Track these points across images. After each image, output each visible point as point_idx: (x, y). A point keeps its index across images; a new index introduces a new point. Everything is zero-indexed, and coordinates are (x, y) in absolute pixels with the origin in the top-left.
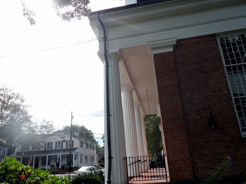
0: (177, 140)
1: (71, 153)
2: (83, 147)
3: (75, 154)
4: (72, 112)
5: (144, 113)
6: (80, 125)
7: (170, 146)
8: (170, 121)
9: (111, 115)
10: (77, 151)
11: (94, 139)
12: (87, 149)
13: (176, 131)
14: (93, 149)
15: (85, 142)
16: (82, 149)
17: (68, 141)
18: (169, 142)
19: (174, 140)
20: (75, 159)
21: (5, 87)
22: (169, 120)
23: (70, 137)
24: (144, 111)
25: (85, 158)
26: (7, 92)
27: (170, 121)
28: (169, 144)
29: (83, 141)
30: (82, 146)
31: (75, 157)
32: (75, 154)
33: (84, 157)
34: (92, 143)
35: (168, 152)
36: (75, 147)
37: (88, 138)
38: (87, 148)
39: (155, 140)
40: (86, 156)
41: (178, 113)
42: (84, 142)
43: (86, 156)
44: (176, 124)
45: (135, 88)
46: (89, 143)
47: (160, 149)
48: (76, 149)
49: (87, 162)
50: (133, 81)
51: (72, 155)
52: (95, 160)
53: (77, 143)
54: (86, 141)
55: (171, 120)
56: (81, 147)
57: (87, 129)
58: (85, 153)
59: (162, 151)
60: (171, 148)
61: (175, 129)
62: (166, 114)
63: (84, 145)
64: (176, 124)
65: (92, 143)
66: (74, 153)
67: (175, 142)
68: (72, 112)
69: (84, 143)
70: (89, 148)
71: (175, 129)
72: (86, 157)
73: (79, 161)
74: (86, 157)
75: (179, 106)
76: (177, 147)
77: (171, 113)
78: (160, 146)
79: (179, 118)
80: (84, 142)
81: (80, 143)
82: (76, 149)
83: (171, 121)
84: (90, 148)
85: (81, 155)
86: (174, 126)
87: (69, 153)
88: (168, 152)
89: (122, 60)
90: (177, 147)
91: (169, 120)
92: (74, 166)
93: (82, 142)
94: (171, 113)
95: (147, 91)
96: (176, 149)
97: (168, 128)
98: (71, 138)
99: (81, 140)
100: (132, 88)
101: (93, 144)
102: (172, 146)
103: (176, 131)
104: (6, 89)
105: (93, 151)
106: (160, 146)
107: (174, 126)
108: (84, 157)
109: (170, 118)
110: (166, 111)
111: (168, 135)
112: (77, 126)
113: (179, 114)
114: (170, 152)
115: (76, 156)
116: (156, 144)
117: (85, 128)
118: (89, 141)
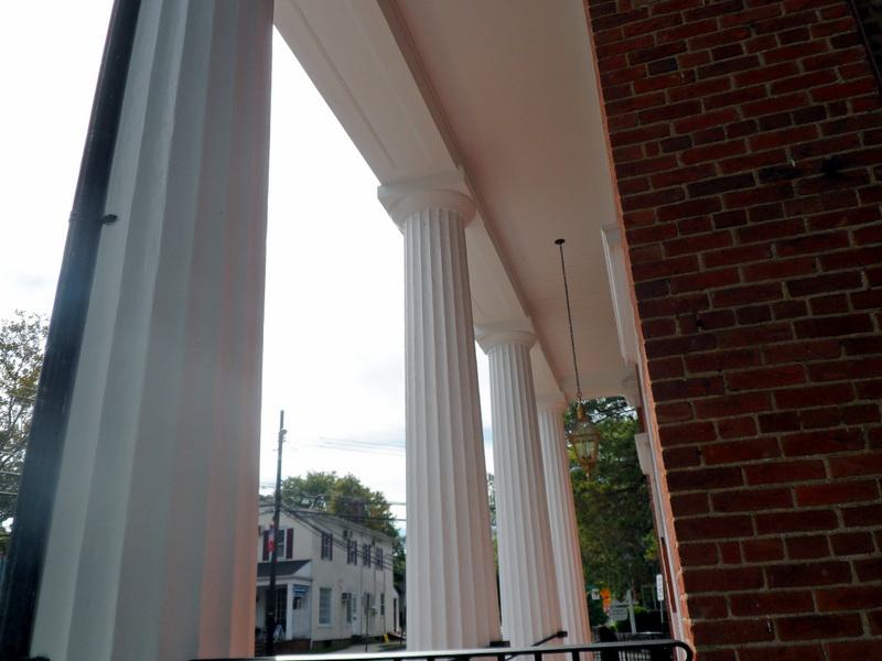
0: (843, 441)
1: (273, 581)
2: (331, 558)
3: (295, 585)
4: (282, 413)
5: (561, 389)
6: (341, 474)
7: (741, 526)
8: (724, 221)
9: (113, 218)
10: (303, 572)
11: (391, 528)
12: (352, 564)
13: (806, 329)
14: (380, 564)
15: (341, 539)
16: (326, 562)
17: (286, 532)
18: (731, 476)
19: (795, 447)
20: (295, 606)
21: (26, 319)
22: (714, 205)
23: (273, 515)
24: (560, 380)
25: (343, 602)
26: (33, 338)
27: (724, 221)
28: (721, 503)
29: (335, 536)
30: (326, 553)
31: (296, 599)
32: (295, 585)
33: (335, 599)
34: (373, 543)
35: (717, 608)
36: (296, 556)
37: (356, 520)
38: (352, 558)
39: (622, 524)
40: (345, 596)
41: (818, 113)
42: (337, 534)
43: (345, 596)
44: (799, 245)
45: (540, 336)
46: (360, 541)
47: (650, 569)
48: (302, 563)
49: (349, 619)
50: (530, 306)
51: (284, 590)
52: (386, 611)
53: (305, 543)
54: (345, 534)
55: (740, 147)
56: (323, 557)
57: (368, 490)
58: (341, 581)
59: (659, 577)
60: (753, 552)
61: (798, 309)
62: (671, 145)
63: (339, 553)
64: (799, 245)
65: (373, 543)
66: (289, 583)
67: (818, 470)
68: (282, 413)
69: (338, 542)
70: (360, 560)
71: (798, 309)
72: (346, 598)
73: (316, 616)
74: (346, 598)
75: (831, 50)
76: (848, 544)
77: (737, 130)
78: (649, 556)
79: (832, 170)
80: (337, 534)
81: (320, 539)
82: (302, 563)
83: (736, 219)
84: (365, 564)
85: (325, 592)
86: (775, 270)
87: (267, 583)
88: (717, 608)
89: (479, 219)
90: (848, 544)
91: (714, 205)
92: (289, 636)
93: (327, 540)
94: (737, 130)
95: (560, 242)
96: (840, 572)
97: (704, 301)
98: (276, 519)
99: (323, 529)
100: (528, 332)
101: (377, 544)
102: (766, 524)
103: (806, 329)
104: (31, 327)
105: (379, 573)
106: (649, 556)
107: (775, 270)
108: (335, 599)
109: (718, 185)
110: (670, 113)
111: (708, 385)
112: (329, 477)
113: (829, 129)
114: (742, 605)
115: (301, 596)
116: (630, 544)
117: (359, 487)
118: (362, 534)
